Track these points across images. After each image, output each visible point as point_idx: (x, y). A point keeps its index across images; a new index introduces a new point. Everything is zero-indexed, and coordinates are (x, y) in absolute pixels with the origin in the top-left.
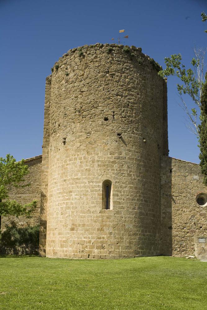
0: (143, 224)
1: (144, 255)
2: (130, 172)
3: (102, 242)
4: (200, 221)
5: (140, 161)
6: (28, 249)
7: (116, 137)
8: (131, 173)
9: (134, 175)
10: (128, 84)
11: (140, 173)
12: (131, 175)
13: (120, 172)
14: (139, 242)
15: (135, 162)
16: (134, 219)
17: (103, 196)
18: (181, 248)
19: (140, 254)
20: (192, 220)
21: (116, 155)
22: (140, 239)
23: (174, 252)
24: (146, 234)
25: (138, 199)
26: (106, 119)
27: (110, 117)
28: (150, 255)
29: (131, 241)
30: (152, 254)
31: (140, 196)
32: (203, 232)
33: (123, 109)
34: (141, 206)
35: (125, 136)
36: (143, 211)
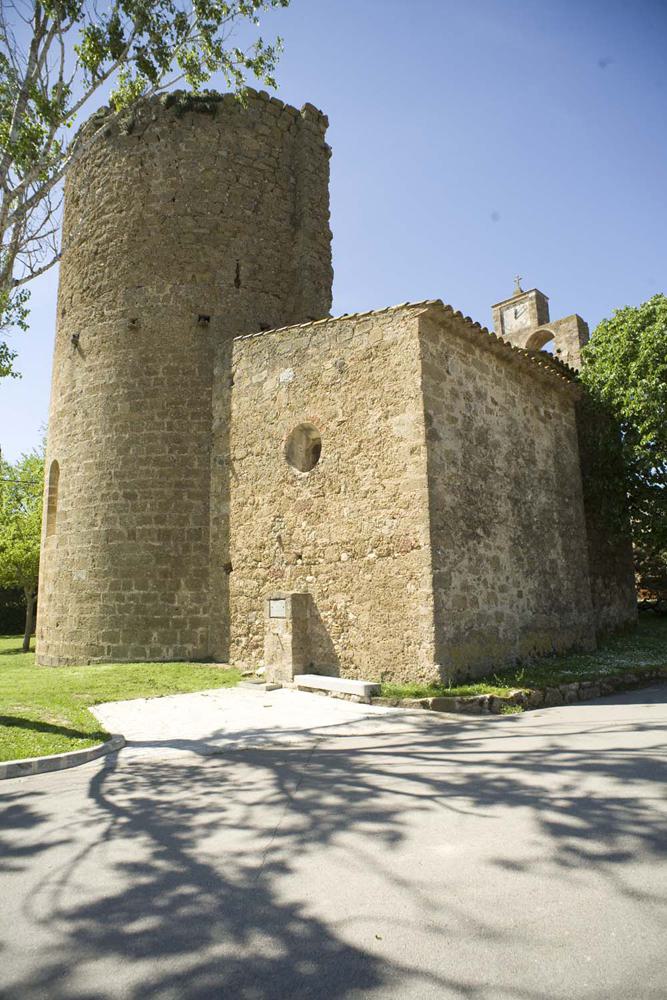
0: (116, 565)
1: (117, 656)
5: (115, 386)
6: (447, 625)
9: (96, 431)
11: (113, 420)
14: (104, 618)
16: (92, 554)
18: (251, 635)
19: (103, 654)
21: (68, 392)
22: (105, 609)
23: (235, 651)
24: (127, 594)
25: (103, 495)
28: (143, 658)
29: (83, 616)
30: (151, 656)
31: (109, 485)
32: (305, 575)
34: (111, 515)
36: (118, 527)
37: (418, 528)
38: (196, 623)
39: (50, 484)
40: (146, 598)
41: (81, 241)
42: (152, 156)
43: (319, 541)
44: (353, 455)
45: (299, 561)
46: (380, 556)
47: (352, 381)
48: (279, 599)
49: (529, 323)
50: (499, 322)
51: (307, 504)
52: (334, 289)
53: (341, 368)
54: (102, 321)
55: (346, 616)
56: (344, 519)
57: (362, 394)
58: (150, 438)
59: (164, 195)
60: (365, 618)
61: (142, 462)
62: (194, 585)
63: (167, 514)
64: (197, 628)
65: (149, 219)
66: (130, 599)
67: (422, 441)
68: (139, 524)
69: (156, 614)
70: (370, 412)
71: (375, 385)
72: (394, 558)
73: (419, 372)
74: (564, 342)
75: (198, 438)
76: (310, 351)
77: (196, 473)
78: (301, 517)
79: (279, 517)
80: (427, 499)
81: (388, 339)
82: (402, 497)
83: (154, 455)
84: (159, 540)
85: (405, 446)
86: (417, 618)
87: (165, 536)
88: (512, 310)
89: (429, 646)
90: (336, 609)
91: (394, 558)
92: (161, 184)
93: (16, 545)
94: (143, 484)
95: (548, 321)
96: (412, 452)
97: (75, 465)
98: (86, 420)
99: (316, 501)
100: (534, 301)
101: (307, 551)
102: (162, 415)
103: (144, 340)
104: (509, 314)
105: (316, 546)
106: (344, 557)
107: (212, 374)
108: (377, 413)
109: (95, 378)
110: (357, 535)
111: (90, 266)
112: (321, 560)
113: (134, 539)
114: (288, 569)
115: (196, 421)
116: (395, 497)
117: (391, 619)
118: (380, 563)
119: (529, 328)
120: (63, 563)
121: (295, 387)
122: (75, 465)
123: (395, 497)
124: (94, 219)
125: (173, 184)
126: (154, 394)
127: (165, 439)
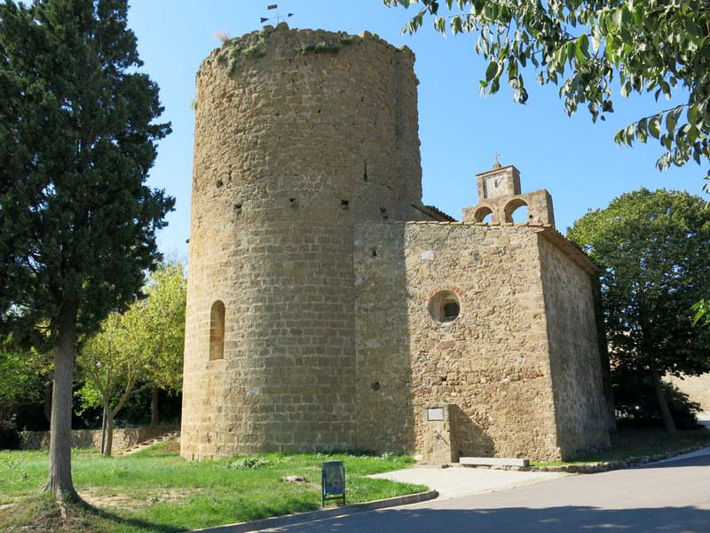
2: (258, 276)
3: (208, 429)
4: (441, 361)
7: (231, 214)
8: (259, 279)
9: (264, 281)
10: (256, 104)
12: (257, 283)
13: (237, 283)
15: (267, 253)
17: (548, 339)
20: (421, 362)
21: (233, 248)
26: (220, 184)
27: (225, 179)
32: (450, 391)
33: (245, 154)
35: (247, 208)
37: (541, 363)
38: (348, 427)
39: (212, 319)
40: (311, 408)
41: (237, 131)
42: (302, 76)
43: (461, 369)
44: (488, 315)
45: (444, 383)
46: (512, 380)
47: (486, 267)
48: (437, 408)
49: (507, 192)
50: (482, 188)
51: (451, 344)
52: (422, 182)
53: (476, 256)
54: (265, 198)
55: (487, 419)
56: (479, 355)
57: (494, 276)
58: (310, 289)
59: (312, 107)
60: (502, 419)
61: (305, 307)
62: (346, 399)
63: (326, 346)
64: (349, 430)
65: (302, 124)
66: (299, 409)
67: (543, 310)
68: (305, 353)
69: (320, 420)
70: (501, 289)
71: (505, 271)
72: (524, 382)
73: (539, 267)
74: (535, 210)
75: (345, 291)
76: (448, 242)
77: (344, 317)
78: (444, 353)
79: (425, 352)
80: (547, 346)
81: (514, 243)
82: (528, 344)
83: (313, 302)
84: (321, 365)
85: (531, 312)
86: (543, 419)
87: (324, 362)
88: (493, 179)
89: (552, 436)
90: (477, 414)
91: (524, 382)
92: (310, 98)
93: (455, 373)
94: (307, 324)
95: (520, 193)
96: (535, 317)
97: (244, 306)
98: (254, 273)
99: (458, 343)
100: (511, 175)
101: (451, 376)
102: (319, 273)
103: (303, 215)
104: (490, 182)
105: (459, 372)
106: (483, 380)
107: (353, 245)
108: (506, 289)
109: (261, 242)
110: (493, 366)
111: (250, 152)
112: (464, 382)
113: (301, 364)
114: (435, 387)
115: (343, 278)
116: (523, 343)
117: (523, 420)
118: (513, 385)
119: (506, 196)
120: (235, 382)
121: (436, 265)
122: (244, 306)
123: (523, 343)
124: (251, 116)
125: (319, 100)
126: (312, 256)
127: (321, 290)
